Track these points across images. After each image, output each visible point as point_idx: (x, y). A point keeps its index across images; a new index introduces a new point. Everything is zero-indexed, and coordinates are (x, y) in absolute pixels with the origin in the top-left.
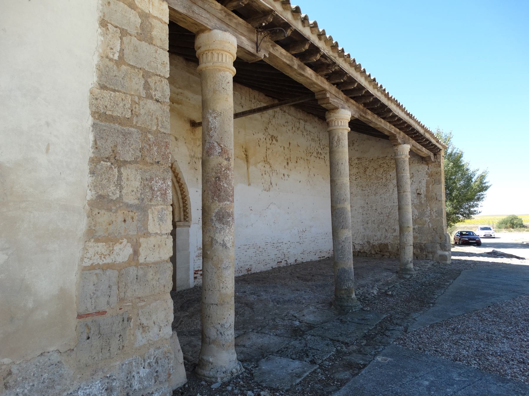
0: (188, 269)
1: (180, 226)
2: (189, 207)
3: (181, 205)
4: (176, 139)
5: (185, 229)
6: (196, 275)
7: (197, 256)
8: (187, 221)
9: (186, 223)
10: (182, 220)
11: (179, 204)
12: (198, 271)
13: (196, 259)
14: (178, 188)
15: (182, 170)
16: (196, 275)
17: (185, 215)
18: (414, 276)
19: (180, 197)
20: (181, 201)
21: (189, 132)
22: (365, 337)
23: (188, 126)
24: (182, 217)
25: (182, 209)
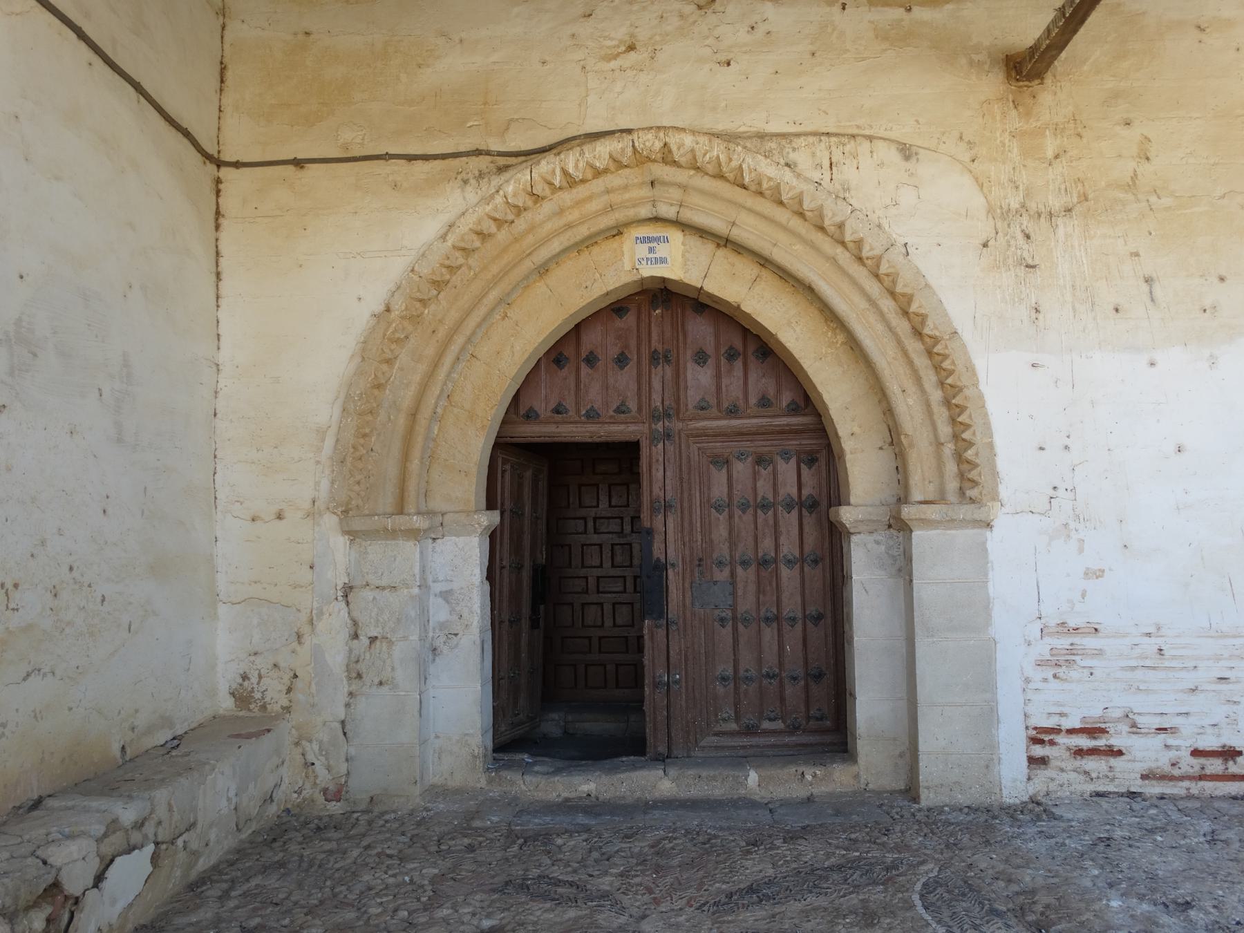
0: (989, 716)
1: (927, 523)
2: (979, 439)
3: (945, 430)
4: (907, 152)
5: (964, 536)
6: (1038, 751)
7: (1040, 664)
8: (972, 501)
9: (965, 511)
10: (952, 496)
11: (935, 429)
12: (1056, 731)
13: (1037, 675)
14: (921, 362)
15: (935, 278)
16: (1038, 751)
17: (962, 476)
18: (325, 739)
19: (936, 395)
20: (941, 414)
21: (996, 108)
22: (473, 851)
23: (993, 84)
24: (952, 485)
25: (949, 449)
